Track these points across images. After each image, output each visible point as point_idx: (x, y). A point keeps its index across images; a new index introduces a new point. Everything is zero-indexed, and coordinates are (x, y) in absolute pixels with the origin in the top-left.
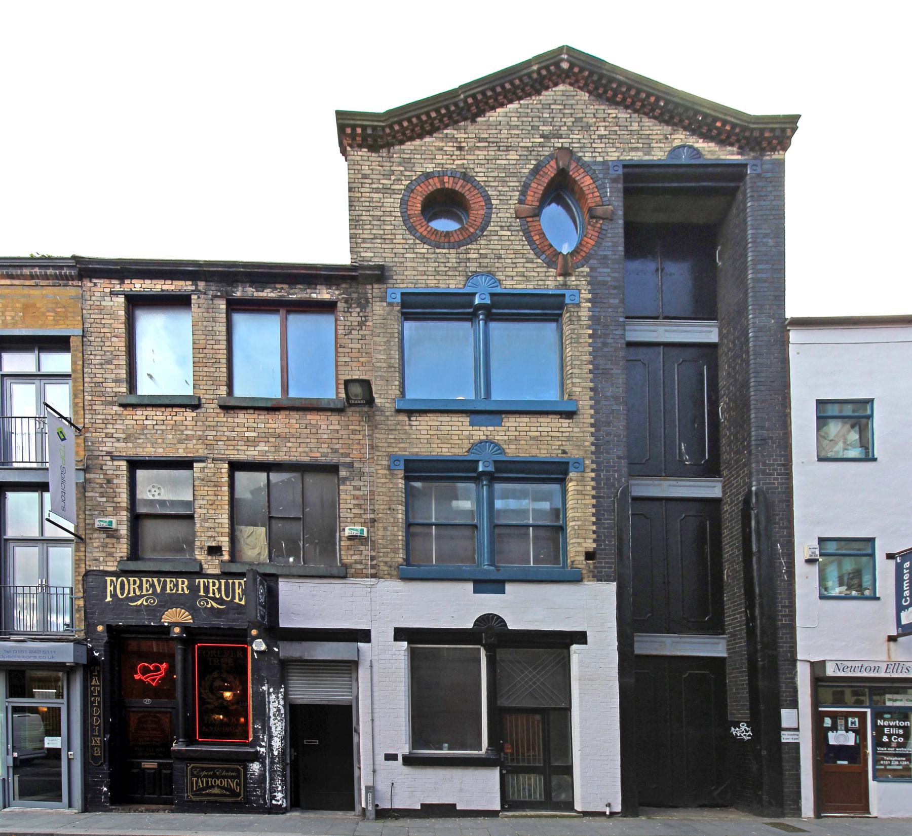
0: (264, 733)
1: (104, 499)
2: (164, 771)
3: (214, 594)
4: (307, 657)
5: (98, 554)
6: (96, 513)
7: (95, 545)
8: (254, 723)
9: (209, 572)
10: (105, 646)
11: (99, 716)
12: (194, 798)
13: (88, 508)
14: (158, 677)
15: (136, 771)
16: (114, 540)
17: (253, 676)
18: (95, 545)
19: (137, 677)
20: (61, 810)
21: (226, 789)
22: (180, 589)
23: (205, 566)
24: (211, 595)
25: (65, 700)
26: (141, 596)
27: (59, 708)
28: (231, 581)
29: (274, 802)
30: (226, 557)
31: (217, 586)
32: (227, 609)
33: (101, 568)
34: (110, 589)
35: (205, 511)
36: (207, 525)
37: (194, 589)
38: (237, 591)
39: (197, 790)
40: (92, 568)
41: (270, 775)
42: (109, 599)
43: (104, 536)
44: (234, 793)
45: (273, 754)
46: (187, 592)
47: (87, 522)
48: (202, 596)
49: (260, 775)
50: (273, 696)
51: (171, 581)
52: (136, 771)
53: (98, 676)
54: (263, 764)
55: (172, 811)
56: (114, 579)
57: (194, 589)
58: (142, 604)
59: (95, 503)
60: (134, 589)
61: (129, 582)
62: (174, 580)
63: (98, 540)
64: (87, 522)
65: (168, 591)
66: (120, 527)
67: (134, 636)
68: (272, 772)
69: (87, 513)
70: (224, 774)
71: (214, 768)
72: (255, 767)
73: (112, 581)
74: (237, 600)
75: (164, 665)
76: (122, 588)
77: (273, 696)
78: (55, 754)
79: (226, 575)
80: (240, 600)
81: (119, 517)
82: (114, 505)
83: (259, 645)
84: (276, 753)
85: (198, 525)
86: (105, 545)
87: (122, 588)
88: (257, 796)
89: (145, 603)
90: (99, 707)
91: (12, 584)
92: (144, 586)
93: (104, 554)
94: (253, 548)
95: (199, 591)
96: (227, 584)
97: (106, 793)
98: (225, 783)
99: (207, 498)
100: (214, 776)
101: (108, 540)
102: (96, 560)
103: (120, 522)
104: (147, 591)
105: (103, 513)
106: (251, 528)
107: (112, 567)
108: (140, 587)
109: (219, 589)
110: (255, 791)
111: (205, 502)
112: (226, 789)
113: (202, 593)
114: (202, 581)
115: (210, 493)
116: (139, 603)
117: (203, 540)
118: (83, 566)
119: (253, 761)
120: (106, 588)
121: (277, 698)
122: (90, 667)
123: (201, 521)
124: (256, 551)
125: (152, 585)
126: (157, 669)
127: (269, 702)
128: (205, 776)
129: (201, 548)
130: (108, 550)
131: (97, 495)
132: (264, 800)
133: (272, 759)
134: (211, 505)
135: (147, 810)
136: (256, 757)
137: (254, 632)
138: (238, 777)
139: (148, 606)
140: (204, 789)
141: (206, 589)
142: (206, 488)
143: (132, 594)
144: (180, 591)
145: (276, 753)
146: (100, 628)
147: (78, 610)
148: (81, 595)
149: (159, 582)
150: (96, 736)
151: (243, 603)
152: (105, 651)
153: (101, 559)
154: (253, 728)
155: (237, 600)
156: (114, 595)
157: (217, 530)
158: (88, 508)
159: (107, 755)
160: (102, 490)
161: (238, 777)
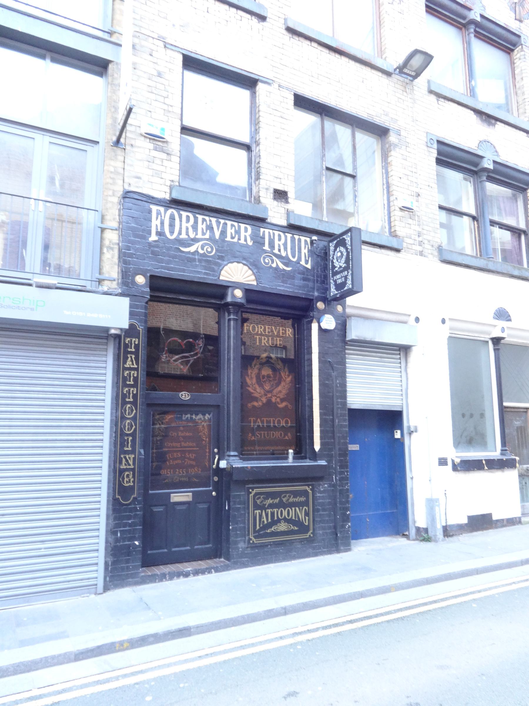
4: (377, 340)
9: (274, 221)
11: (134, 419)
16: (164, 156)
23: (270, 213)
24: (276, 251)
26: (195, 240)
34: (155, 223)
37: (258, 241)
39: (261, 529)
42: (154, 237)
43: (151, 146)
52: (160, 509)
56: (162, 209)
57: (258, 241)
58: (197, 251)
60: (187, 229)
61: (180, 216)
70: (291, 500)
73: (158, 213)
74: (303, 263)
76: (172, 226)
82: (166, 107)
87: (172, 226)
90: (134, 403)
95: (263, 244)
96: (293, 239)
100: (282, 505)
104: (204, 234)
108: (195, 227)
109: (285, 245)
113: (266, 247)
114: (267, 231)
116: (192, 249)
125: (210, 228)
128: (271, 506)
129: (267, 189)
130: (154, 166)
138: (306, 503)
139: (204, 255)
140: (265, 527)
144: (242, 241)
146: (140, 280)
148: (115, 225)
149: (218, 223)
151: (309, 266)
161: (306, 503)
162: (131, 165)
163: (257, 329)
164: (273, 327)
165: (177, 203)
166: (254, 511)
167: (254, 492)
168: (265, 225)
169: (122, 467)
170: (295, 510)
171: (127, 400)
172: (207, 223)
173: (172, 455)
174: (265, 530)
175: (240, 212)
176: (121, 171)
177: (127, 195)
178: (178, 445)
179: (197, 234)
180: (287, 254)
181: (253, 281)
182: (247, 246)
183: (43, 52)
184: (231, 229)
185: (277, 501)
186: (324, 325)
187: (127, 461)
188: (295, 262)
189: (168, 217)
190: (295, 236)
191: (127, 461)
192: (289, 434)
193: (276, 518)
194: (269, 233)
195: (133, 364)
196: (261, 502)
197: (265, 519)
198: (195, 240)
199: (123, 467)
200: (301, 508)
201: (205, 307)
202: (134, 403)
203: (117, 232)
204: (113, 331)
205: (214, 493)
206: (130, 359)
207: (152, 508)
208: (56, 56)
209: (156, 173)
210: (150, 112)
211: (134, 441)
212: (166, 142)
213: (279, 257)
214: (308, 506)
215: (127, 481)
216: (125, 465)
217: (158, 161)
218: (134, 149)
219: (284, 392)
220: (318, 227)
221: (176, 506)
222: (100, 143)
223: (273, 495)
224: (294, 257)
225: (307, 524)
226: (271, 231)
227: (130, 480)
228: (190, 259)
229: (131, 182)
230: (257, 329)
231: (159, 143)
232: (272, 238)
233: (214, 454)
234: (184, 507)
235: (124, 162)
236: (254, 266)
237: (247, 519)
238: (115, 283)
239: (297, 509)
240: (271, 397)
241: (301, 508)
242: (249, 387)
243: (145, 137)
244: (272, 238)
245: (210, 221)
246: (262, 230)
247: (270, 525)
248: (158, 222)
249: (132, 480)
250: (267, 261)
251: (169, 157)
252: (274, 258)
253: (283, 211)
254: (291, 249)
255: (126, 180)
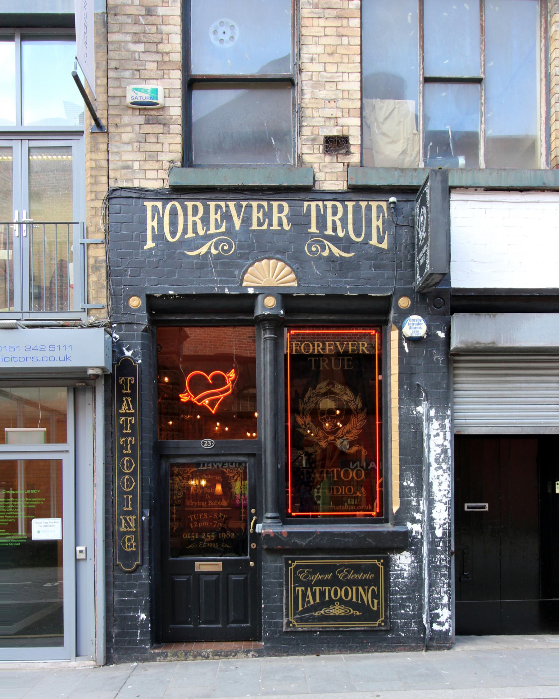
0: (419, 495)
1: (141, 47)
2: (234, 577)
3: (334, 229)
4: (504, 343)
5: (131, 157)
6: (127, 74)
7: (126, 137)
8: (402, 477)
9: (327, 186)
10: (143, 338)
11: (134, 474)
12: (300, 628)
13: (113, 64)
14: (222, 396)
15: (183, 578)
16: (159, 129)
17: (401, 386)
18: (126, 137)
19: (184, 398)
20: (64, 664)
21: (355, 606)
22: (275, 222)
23: (320, 176)
24: (329, 232)
25: (70, 446)
26: (207, 237)
27: (59, 463)
28: (363, 204)
29: (435, 627)
30: (355, 158)
31: (340, 214)
32: (358, 258)
33: (136, 184)
34: (151, 224)
35: (320, 68)
36: (323, 94)
37: (299, 221)
38: (375, 223)
39: (305, 611)
40: (120, 185)
41: (430, 575)
42: (150, 244)
43: (141, 119)
44: (369, 614)
45: (434, 534)
46: (287, 227)
47: (111, 92)
48: (313, 235)
49: (411, 577)
50: (436, 424)
51: (260, 207)
52: (183, 578)
53: (132, 395)
54: (417, 554)
55: (260, 653)
56: (159, 204)
57: (299, 221)
58: (208, 252)
59: (125, 54)
60: (195, 224)
61: (185, 209)
62: (265, 204)
63: (129, 128)
64: (111, 92)
65: (255, 227)
66: (169, 102)
67: (185, 318)
68: (434, 568)
69: (111, 74)
70: (351, 576)
71: (335, 567)
72: (403, 561)
73: (155, 208)
74: (374, 242)
75: (232, 374)
76: (173, 224)
77: (436, 424)
78: (50, 553)
79: (359, 191)
80: (380, 240)
81: (167, 83)
82: (158, 58)
83: (416, 326)
84: (439, 533)
85: (307, 96)
86: (143, 139)
87: (173, 224)
88: (405, 616)
89: (214, 252)
90: (133, 455)
91: (321, 146)
92: (213, 217)
93: (140, 156)
94: (393, 142)
95: (309, 225)
96: (357, 210)
97: (143, 625)
98: (352, 594)
99: (324, 41)
100: (335, 582)
101: (148, 129)
102: (127, 168)
103: (167, 90)
104: (217, 226)
105: (139, 74)
106: (390, 104)
107: (155, 180)
108: (205, 220)
109: (344, 221)
110: (403, 607)
111: (320, 50)
112: (355, 606)
113: (313, 229)
114: (313, 204)
115: (329, 31)
116: (203, 250)
117: (319, 122)
118: (105, 179)
119: (399, 550)
120: (145, 223)
121: (443, 427)
122: (117, 377)
123: (313, 87)
124: (399, 147)
125: (227, 216)
126: (219, 381)
127: (429, 436)
128: (320, 583)
129: (314, 140)
130: (148, 147)
131: (129, 38)
132: (420, 623)
133: (433, 543)
134: (331, 54)
135: (217, 654)
136: (404, 542)
137: (404, 302)
138: (375, 582)
139: (218, 256)
140: (316, 607)
141: (322, 223)
142: (322, 22)
143: (190, 234)
144: (275, 227)
145: (439, 533)
146: (135, 302)
147: (96, 269)
148: (100, 237)
149: (239, 208)
150: (129, 513)
151: (384, 245)
152: (143, 346)
153: (136, 166)
154: (401, 487)
155: (374, 242)
156: (159, 237)
157: (341, 104)
158: (113, 64)
159: (146, 549)
160: (137, 29)
161: (375, 582)
162: (118, 153)
163: (312, 348)
164: (338, 343)
165: (180, 191)
166: (295, 588)
167: (295, 564)
168: (311, 196)
169: (122, 530)
170: (357, 590)
171: (125, 452)
172: (222, 211)
173: (196, 517)
174: (312, 612)
175: (268, 184)
176: (104, 163)
177: (112, 195)
178: (204, 504)
179: (208, 229)
180: (347, 233)
181: (293, 281)
182: (282, 232)
183: (10, 31)
184: (258, 212)
185: (329, 576)
186: (408, 331)
187: (127, 522)
188: (362, 243)
189: (168, 213)
190: (361, 203)
191: (127, 522)
192: (363, 490)
193: (327, 599)
194: (317, 206)
195: (130, 409)
196: (304, 578)
197: (311, 599)
198: (207, 237)
199: (123, 529)
200: (366, 587)
201: (225, 326)
202: (133, 455)
203: (103, 246)
204: (90, 372)
205: (252, 564)
206: (125, 402)
207: (173, 576)
208: (27, 31)
209: (150, 156)
210: (138, 70)
211: (134, 500)
212: (163, 108)
213: (334, 239)
214: (377, 585)
215: (128, 546)
216: (126, 527)
217: (152, 139)
218: (121, 130)
219: (355, 432)
220: (357, 182)
221: (202, 576)
222: (85, 132)
223: (323, 569)
224: (358, 235)
225: (375, 609)
226: (320, 203)
227: (132, 544)
228: (202, 263)
229: (118, 176)
230: (312, 348)
231: (152, 113)
232: (161, 216)
233: (251, 516)
234: (214, 578)
235: (108, 151)
236: (296, 261)
237: (284, 597)
238: (104, 311)
239: (360, 589)
240: (334, 440)
241: (366, 587)
242: (300, 428)
243: (133, 108)
244: (161, 216)
245: (227, 206)
246: (306, 204)
247: (316, 607)
248: (155, 223)
249: (134, 544)
250: (314, 249)
251: (166, 128)
252: (325, 242)
253: (340, 167)
254: (354, 224)
255: (111, 174)
